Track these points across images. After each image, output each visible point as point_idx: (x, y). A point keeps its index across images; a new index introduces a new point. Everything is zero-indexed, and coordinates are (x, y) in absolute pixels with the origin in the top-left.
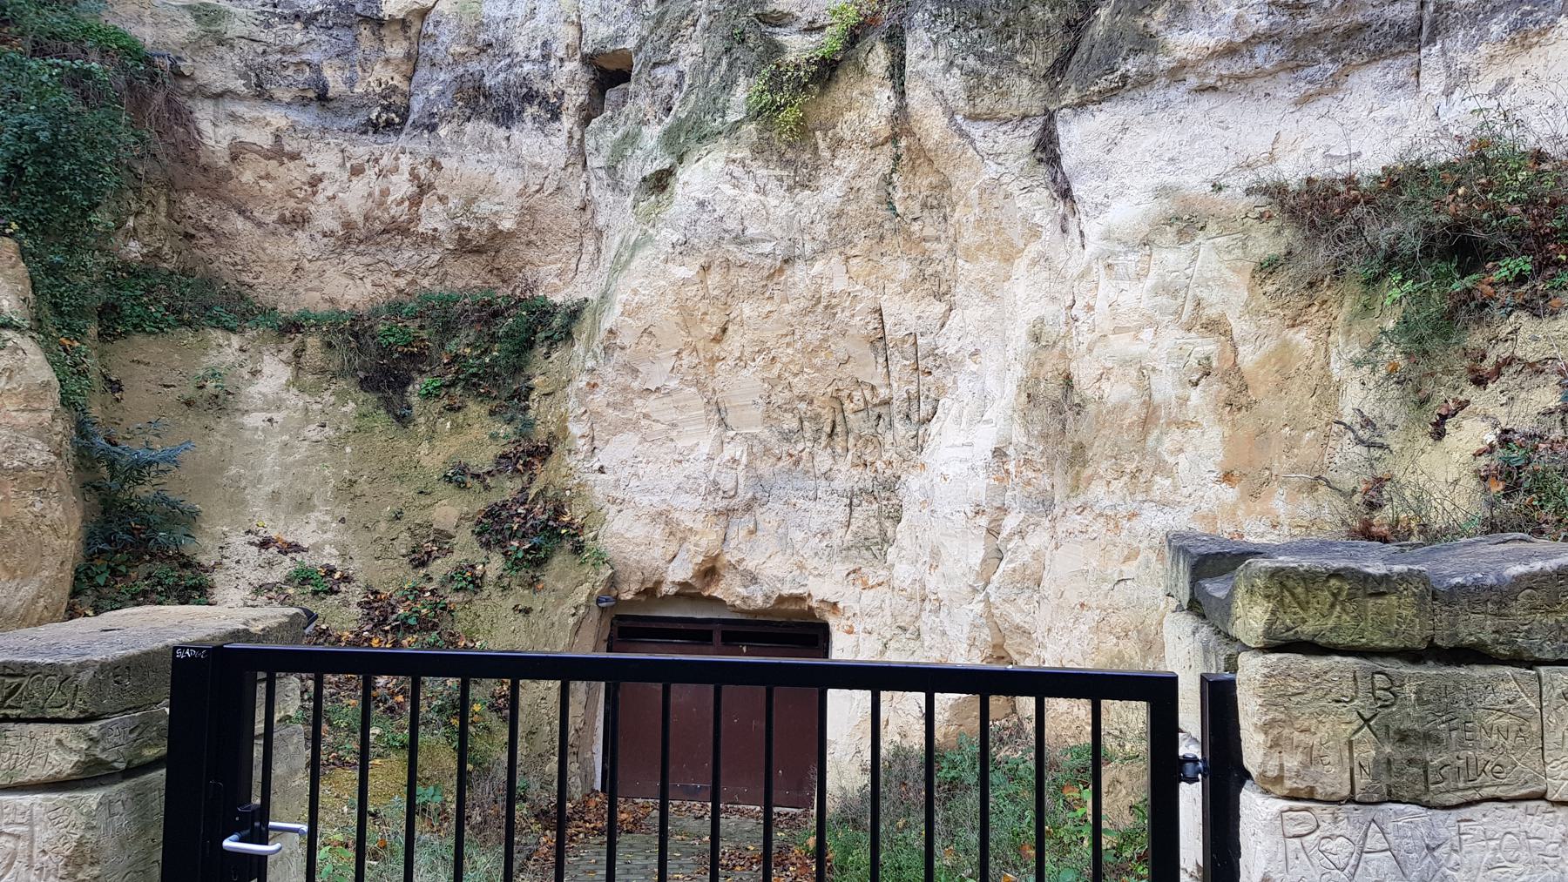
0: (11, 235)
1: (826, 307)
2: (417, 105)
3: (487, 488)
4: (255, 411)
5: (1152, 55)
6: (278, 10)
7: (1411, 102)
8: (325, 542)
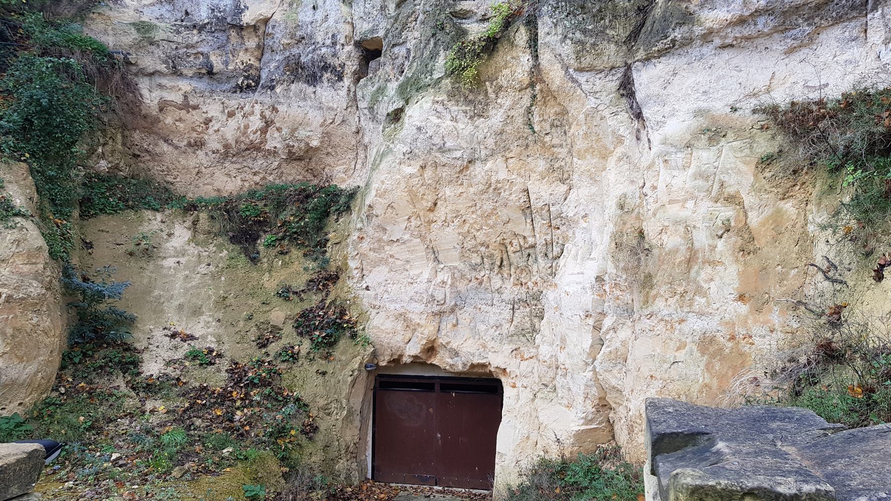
0: (25, 161)
1: (495, 189)
2: (264, 75)
3: (302, 300)
4: (170, 257)
5: (691, 26)
6: (184, 23)
7: (861, 49)
8: (208, 334)
